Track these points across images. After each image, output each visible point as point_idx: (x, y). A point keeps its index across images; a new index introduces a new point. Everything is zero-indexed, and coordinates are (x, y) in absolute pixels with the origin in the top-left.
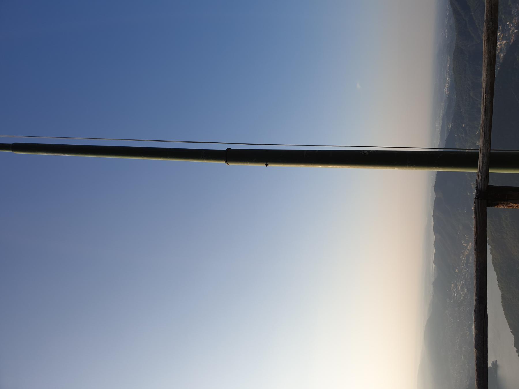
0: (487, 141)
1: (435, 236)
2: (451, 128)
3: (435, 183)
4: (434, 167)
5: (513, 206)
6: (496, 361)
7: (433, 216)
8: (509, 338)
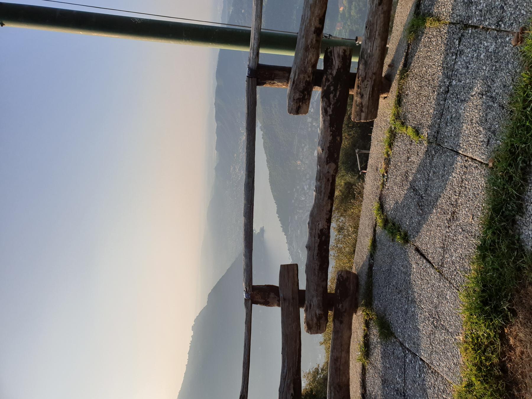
0: (259, 17)
1: (217, 123)
2: (232, 13)
3: (217, 70)
4: (210, 44)
5: (278, 85)
6: (263, 227)
7: (215, 104)
8: (273, 207)
